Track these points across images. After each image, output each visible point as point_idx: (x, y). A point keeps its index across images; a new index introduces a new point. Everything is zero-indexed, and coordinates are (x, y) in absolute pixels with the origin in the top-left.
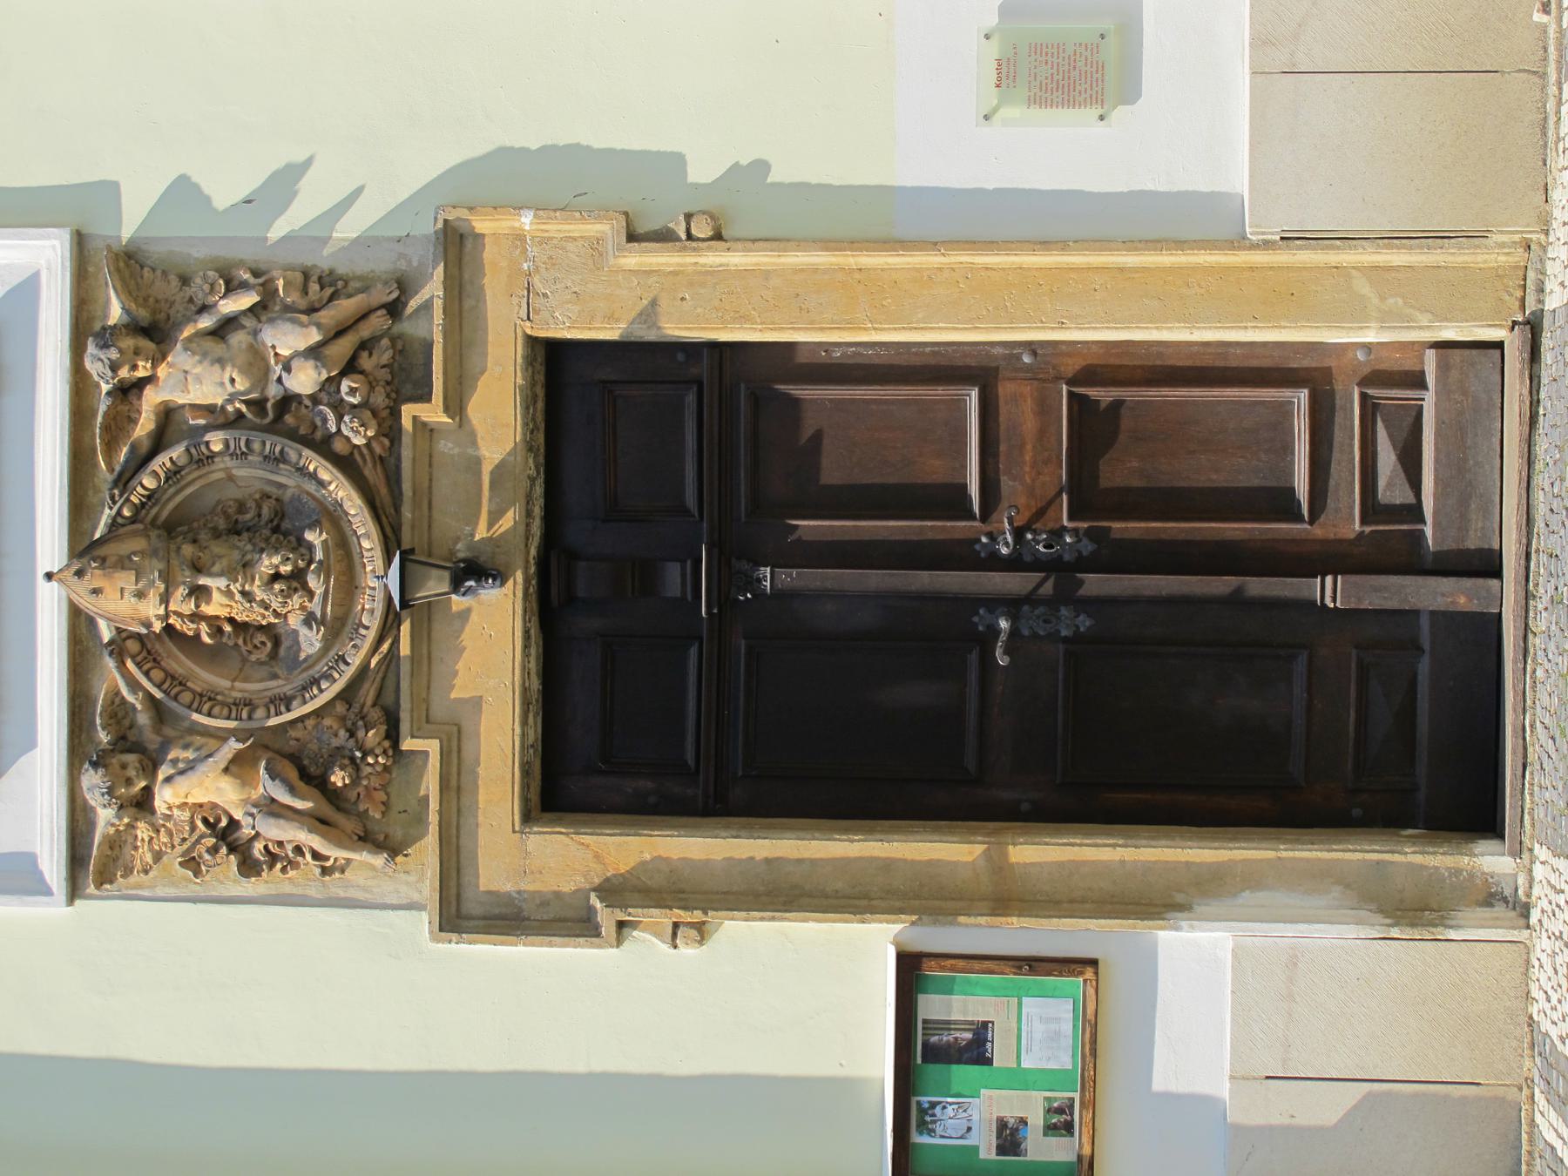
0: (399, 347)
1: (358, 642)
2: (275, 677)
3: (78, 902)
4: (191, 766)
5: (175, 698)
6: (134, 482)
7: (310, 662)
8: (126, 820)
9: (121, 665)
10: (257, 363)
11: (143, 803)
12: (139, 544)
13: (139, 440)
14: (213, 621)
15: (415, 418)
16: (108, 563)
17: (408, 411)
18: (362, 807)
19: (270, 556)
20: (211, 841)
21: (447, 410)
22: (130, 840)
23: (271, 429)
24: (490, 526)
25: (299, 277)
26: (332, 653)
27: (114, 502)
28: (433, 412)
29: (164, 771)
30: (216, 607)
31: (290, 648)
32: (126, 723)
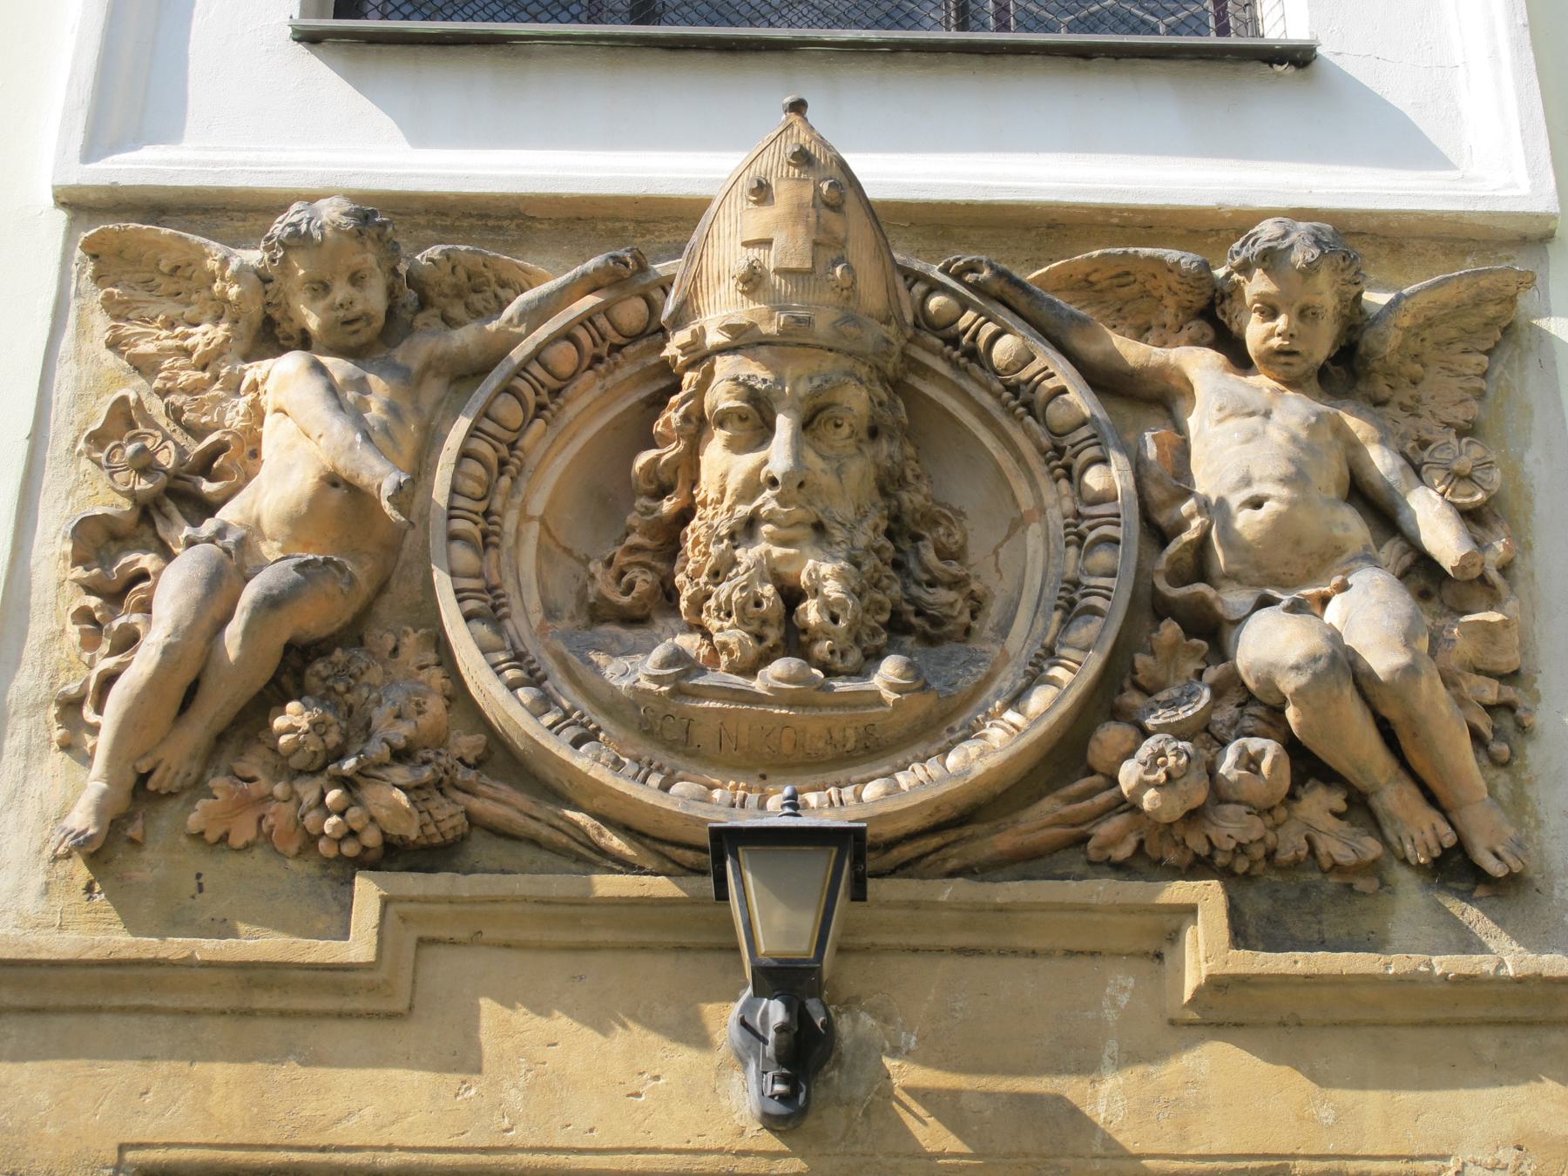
0: (1361, 884)
1: (630, 767)
2: (550, 613)
3: (62, 216)
4: (356, 415)
5: (508, 389)
6: (1005, 316)
7: (584, 672)
8: (233, 291)
9: (591, 284)
10: (1295, 571)
11: (270, 335)
12: (872, 295)
13: (1100, 337)
14: (690, 463)
15: (1190, 911)
16: (827, 214)
17: (1208, 896)
18: (219, 783)
19: (840, 576)
20: (167, 458)
21: (1217, 985)
22: (189, 312)
23: (1150, 606)
24: (922, 1095)
25: (1507, 660)
26: (600, 720)
27: (958, 276)
28: (1205, 952)
29: (339, 367)
30: (721, 465)
31: (618, 638)
32: (457, 311)
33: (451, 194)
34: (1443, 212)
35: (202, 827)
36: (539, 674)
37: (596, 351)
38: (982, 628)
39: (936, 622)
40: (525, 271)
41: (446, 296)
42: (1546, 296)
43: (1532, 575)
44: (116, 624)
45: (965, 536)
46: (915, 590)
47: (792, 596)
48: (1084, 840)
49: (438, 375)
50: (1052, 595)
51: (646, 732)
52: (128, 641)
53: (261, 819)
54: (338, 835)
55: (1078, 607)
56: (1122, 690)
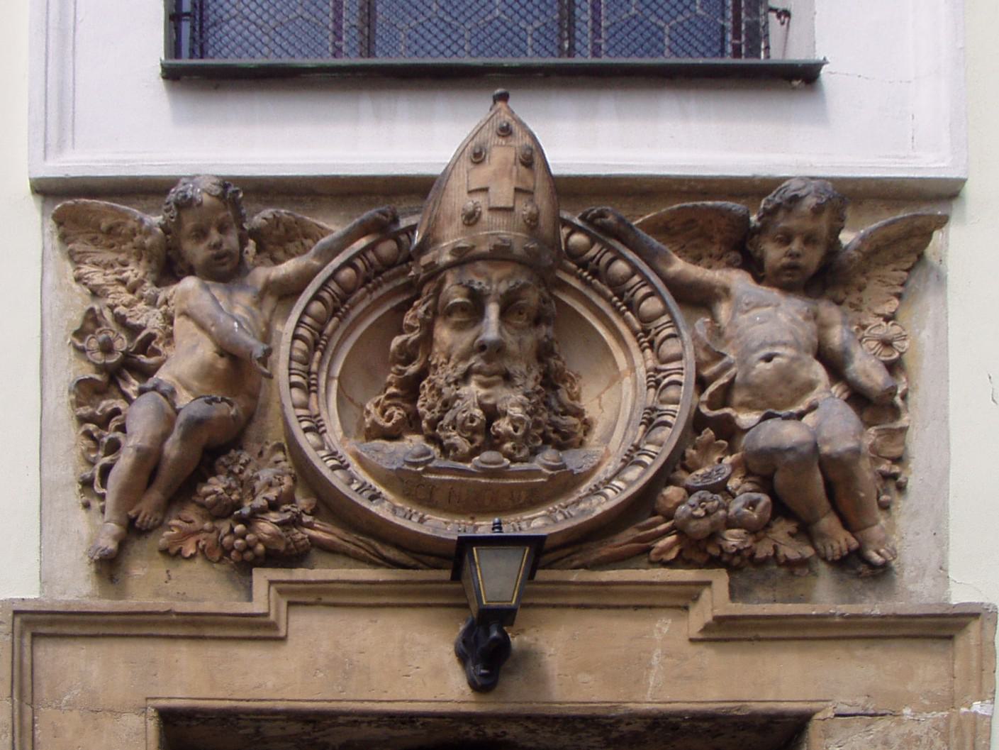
9: (363, 230)
14: (428, 340)
33: (271, 177)
34: (895, 178)
35: (158, 554)
36: (346, 463)
37: (368, 274)
38: (590, 441)
39: (566, 436)
40: (322, 228)
41: (273, 244)
42: (947, 236)
43: (916, 404)
44: (105, 440)
45: (580, 389)
46: (555, 418)
47: (492, 413)
48: (649, 549)
49: (272, 294)
50: (638, 416)
51: (408, 495)
52: (114, 447)
53: (197, 543)
54: (242, 549)
55: (655, 422)
56: (674, 470)
